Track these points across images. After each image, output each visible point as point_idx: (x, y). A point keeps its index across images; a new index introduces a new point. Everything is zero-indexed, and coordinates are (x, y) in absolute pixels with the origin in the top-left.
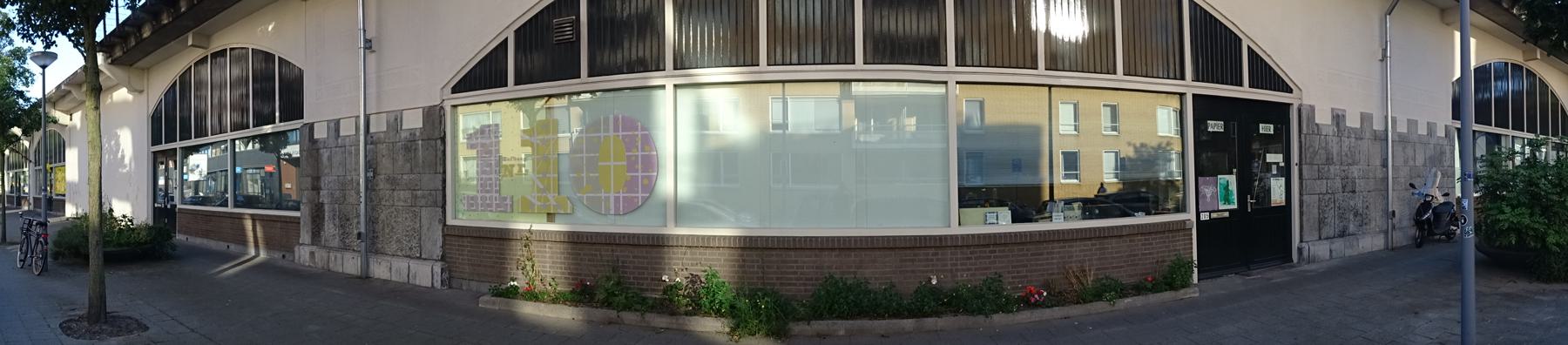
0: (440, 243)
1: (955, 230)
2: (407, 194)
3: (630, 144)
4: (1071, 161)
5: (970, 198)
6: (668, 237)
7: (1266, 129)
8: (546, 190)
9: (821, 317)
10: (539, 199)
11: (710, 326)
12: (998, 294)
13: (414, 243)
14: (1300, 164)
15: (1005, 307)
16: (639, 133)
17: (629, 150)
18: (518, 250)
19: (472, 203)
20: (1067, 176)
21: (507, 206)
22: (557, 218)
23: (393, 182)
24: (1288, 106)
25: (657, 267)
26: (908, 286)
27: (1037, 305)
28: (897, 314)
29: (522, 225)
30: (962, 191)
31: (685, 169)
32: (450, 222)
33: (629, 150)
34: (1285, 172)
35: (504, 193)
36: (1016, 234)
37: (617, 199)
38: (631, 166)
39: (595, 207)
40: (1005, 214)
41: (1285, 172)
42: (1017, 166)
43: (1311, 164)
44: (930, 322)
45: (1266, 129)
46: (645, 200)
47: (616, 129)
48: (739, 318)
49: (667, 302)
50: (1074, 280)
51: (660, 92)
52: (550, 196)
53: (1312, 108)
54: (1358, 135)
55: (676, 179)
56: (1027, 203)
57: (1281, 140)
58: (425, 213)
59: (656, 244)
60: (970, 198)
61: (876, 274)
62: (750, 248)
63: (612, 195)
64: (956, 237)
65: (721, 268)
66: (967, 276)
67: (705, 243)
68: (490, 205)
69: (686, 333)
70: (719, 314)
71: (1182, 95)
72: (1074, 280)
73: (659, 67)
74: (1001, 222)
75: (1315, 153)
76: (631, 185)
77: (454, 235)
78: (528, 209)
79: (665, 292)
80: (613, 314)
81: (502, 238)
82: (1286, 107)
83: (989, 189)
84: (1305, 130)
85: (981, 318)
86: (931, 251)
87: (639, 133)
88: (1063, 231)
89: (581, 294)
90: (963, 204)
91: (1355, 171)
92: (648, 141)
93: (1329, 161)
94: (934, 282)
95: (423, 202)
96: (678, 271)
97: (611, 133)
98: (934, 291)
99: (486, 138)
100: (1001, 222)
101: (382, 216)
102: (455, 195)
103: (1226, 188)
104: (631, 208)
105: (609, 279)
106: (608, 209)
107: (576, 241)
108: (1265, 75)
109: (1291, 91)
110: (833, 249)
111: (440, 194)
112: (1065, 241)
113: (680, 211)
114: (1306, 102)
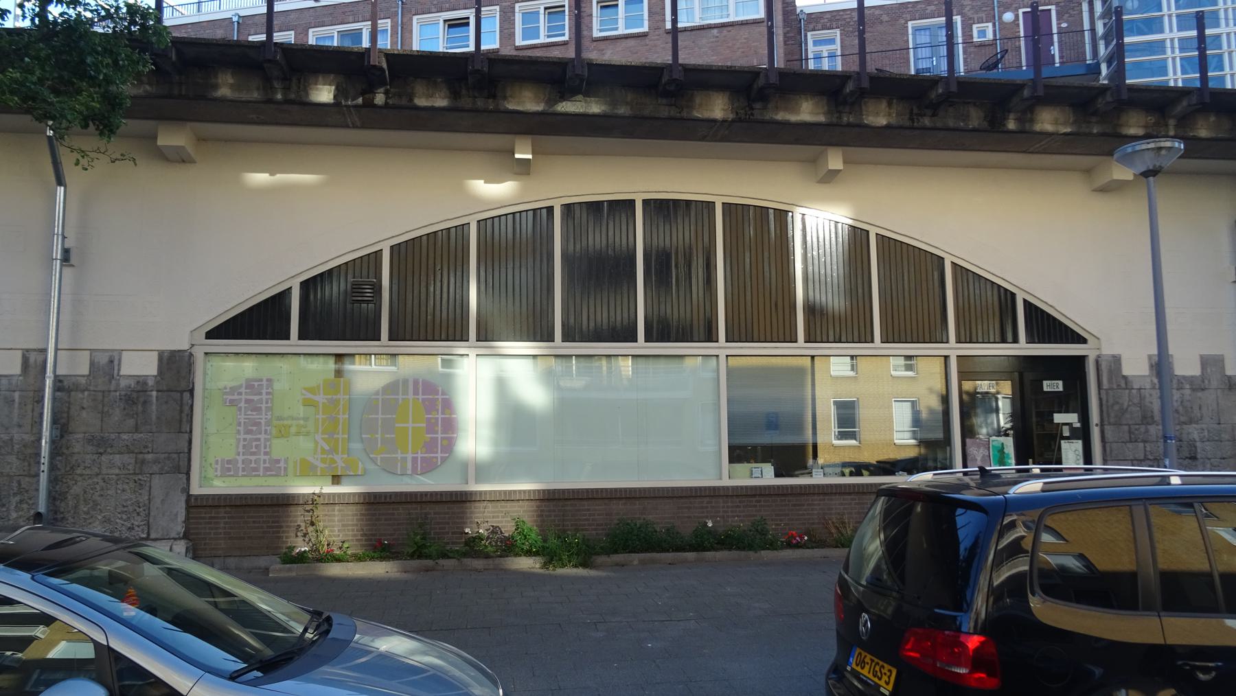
0: (182, 516)
1: (726, 482)
2: (128, 459)
3: (430, 406)
4: (847, 418)
5: (738, 454)
6: (471, 493)
7: (1053, 386)
8: (333, 450)
9: (616, 552)
10: (323, 461)
11: (526, 564)
12: (763, 533)
13: (137, 521)
14: (1102, 425)
15: (772, 545)
16: (440, 397)
17: (428, 411)
18: (299, 517)
19: (228, 468)
20: (842, 436)
21: (275, 468)
22: (344, 480)
23: (101, 444)
24: (1082, 359)
25: (462, 519)
26: (687, 530)
27: (798, 546)
28: (684, 550)
29: (305, 488)
30: (731, 448)
31: (486, 432)
32: (195, 490)
33: (428, 411)
34: (1083, 434)
35: (275, 456)
36: (778, 487)
37: (414, 460)
38: (431, 428)
39: (389, 469)
40: (768, 469)
41: (1083, 434)
42: (772, 423)
43: (1118, 424)
44: (709, 555)
45: (1053, 386)
46: (444, 460)
47: (416, 393)
48: (550, 556)
49: (473, 547)
50: (833, 531)
51: (465, 359)
52: (336, 457)
53: (1117, 360)
54: (1197, 385)
55: (475, 439)
56: (792, 458)
57: (1075, 397)
58: (157, 481)
59: (461, 500)
60: (738, 454)
61: (659, 518)
62: (551, 501)
63: (409, 457)
64: (727, 488)
65: (525, 513)
66: (739, 521)
67: (508, 498)
68: (256, 469)
69: (506, 571)
70: (529, 553)
71: (946, 358)
72: (833, 531)
73: (464, 338)
74: (766, 475)
75: (1123, 411)
76: (430, 446)
77: (199, 507)
78: (307, 471)
79: (466, 544)
80: (429, 563)
81: (283, 503)
82: (1080, 360)
83: (755, 447)
84: (1105, 385)
85: (751, 553)
86: (706, 500)
87: (440, 397)
88: (823, 486)
89: (379, 549)
90: (732, 460)
91: (1194, 432)
92: (448, 405)
93: (1147, 419)
94: (710, 525)
95: (156, 468)
96: (482, 522)
97: (411, 396)
98: (710, 532)
99: (252, 398)
100: (766, 475)
101: (76, 489)
102: (203, 458)
103: (1001, 450)
104: (429, 467)
105: (416, 534)
106: (404, 468)
107: (374, 503)
108: (1045, 325)
109: (1084, 341)
110: (620, 498)
111: (184, 457)
112: (825, 494)
113: (482, 470)
114: (1107, 350)
